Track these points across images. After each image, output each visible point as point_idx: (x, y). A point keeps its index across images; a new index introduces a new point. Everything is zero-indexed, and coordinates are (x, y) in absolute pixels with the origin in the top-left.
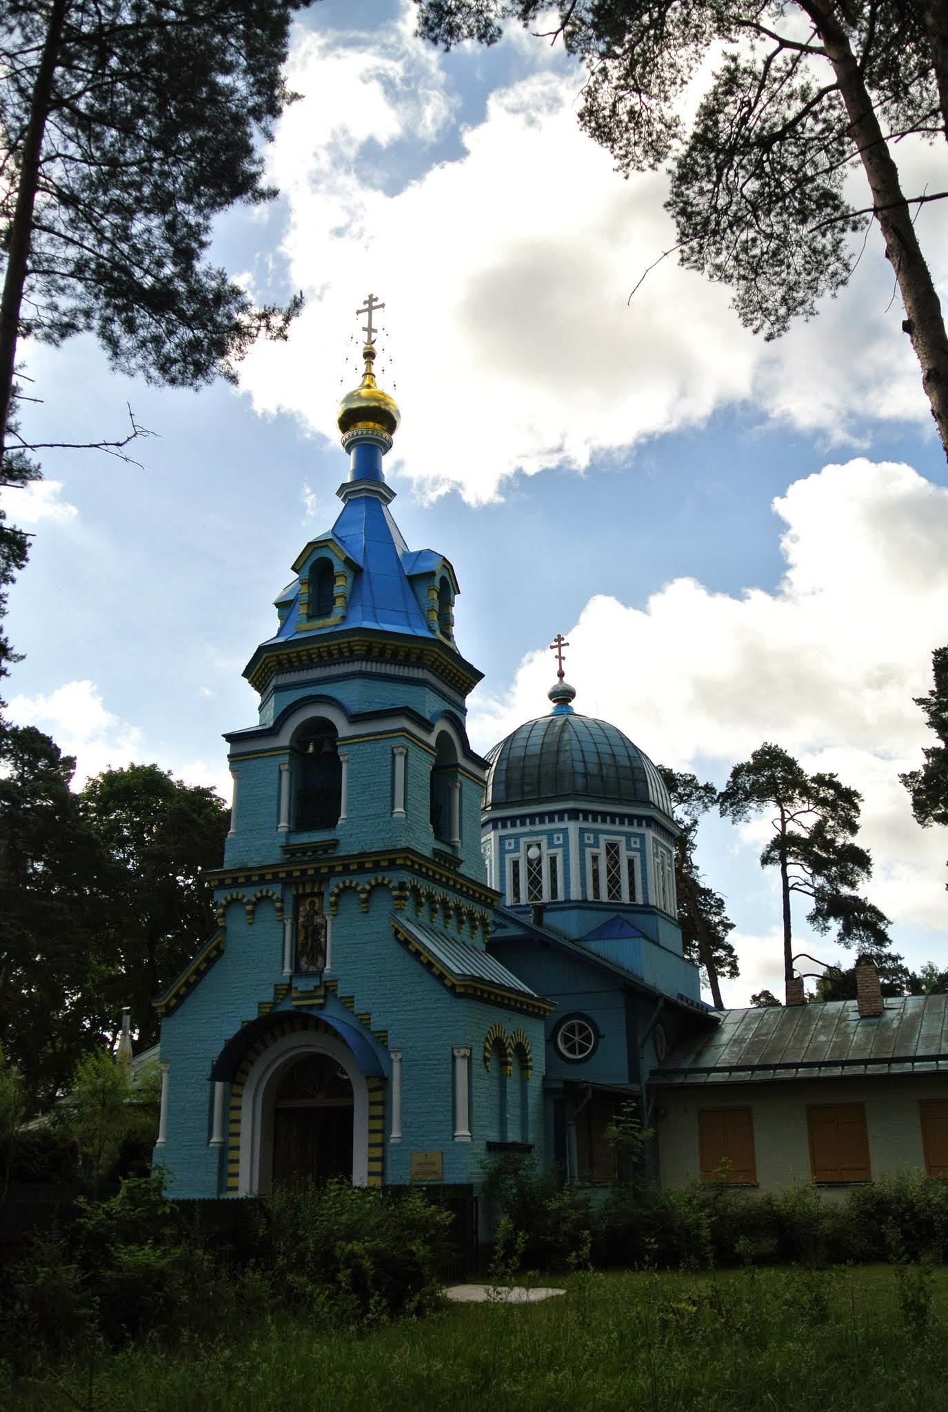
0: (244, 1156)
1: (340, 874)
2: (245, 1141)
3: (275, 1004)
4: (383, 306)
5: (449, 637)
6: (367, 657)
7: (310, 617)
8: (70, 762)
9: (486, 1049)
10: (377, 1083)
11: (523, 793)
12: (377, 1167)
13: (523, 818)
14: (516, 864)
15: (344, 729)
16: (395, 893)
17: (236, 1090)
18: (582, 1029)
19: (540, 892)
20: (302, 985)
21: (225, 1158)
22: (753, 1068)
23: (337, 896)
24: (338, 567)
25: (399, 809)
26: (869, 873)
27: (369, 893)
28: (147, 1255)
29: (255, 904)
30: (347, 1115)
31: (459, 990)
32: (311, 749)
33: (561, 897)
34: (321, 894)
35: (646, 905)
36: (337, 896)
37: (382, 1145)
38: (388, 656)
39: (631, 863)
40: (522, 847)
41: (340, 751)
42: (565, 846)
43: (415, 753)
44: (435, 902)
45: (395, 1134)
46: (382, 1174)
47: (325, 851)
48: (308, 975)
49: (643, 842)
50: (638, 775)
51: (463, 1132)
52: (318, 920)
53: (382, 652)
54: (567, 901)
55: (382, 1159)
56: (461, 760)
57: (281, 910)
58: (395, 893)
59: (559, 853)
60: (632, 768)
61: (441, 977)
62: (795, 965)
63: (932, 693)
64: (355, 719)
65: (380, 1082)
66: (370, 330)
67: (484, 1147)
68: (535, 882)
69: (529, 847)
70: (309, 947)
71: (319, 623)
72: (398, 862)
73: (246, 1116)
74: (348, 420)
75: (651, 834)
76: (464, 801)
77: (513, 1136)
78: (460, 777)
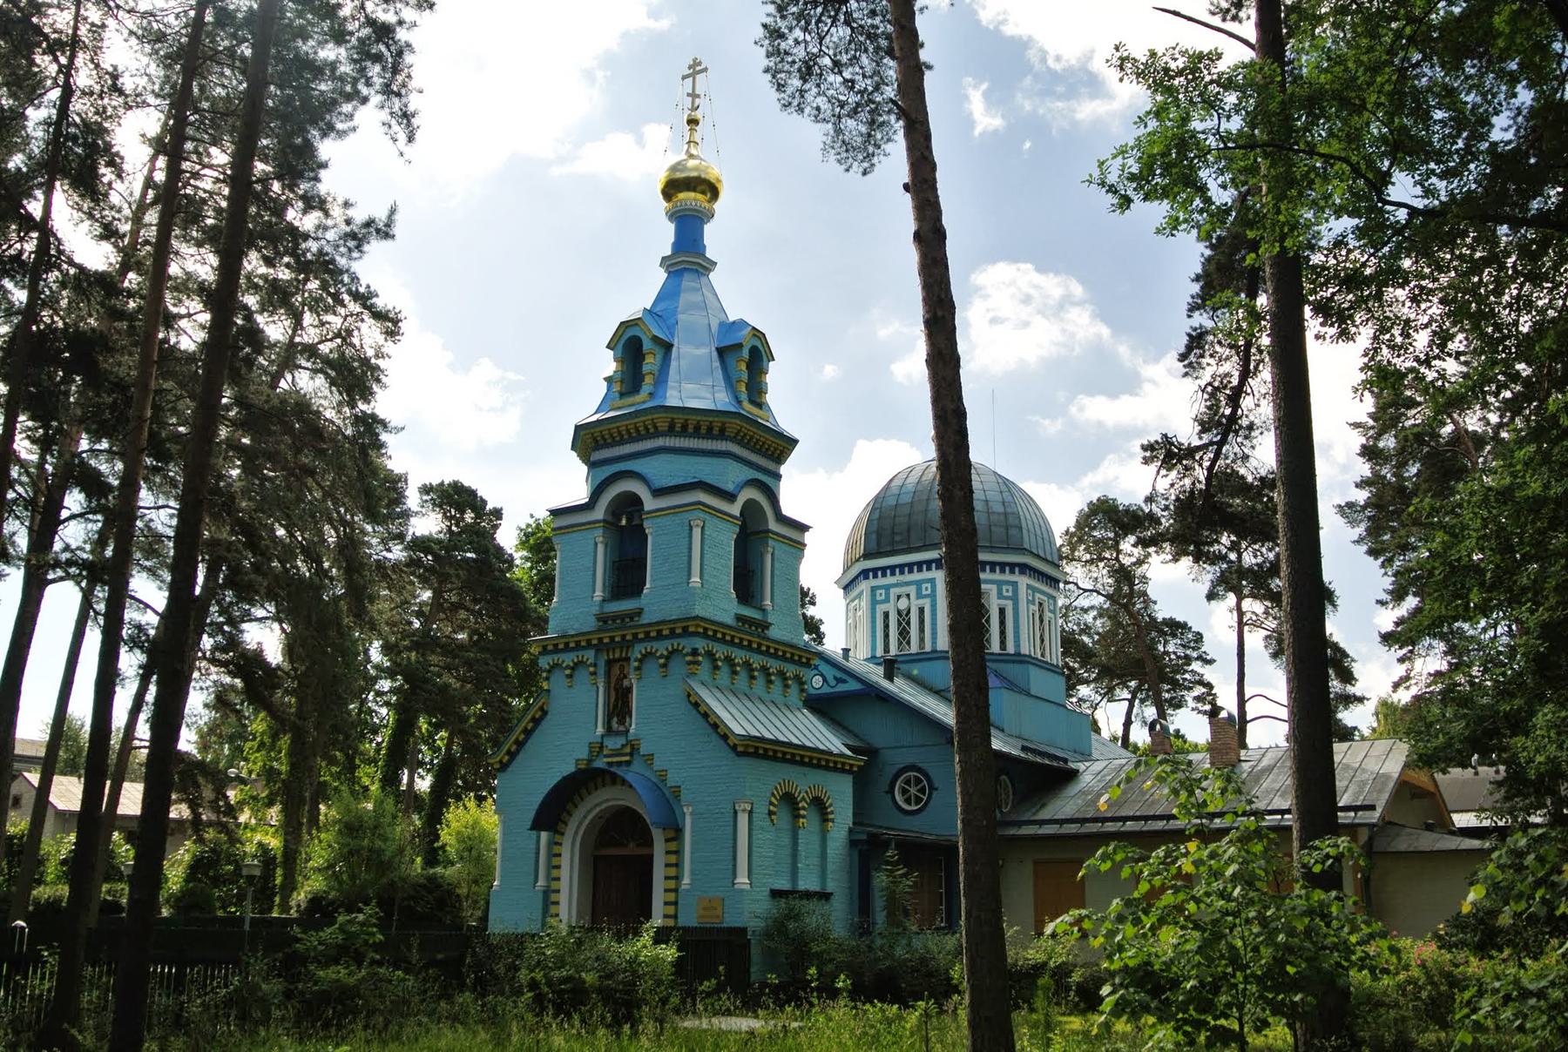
0: (563, 898)
1: (642, 640)
2: (564, 885)
3: (590, 761)
4: (706, 70)
5: (760, 405)
6: (671, 431)
7: (622, 395)
8: (498, 513)
9: (771, 803)
10: (672, 834)
11: (893, 542)
12: (671, 910)
13: (893, 568)
14: (886, 615)
15: (649, 503)
16: (689, 658)
17: (558, 838)
18: (918, 781)
19: (909, 643)
20: (613, 743)
21: (548, 900)
22: (1084, 821)
23: (640, 661)
24: (647, 345)
25: (696, 579)
26: (1335, 606)
27: (667, 658)
28: (338, 973)
29: (573, 669)
30: (648, 861)
31: (740, 749)
32: (624, 522)
33: (928, 648)
34: (627, 659)
35: (1018, 654)
36: (640, 661)
37: (676, 890)
38: (691, 430)
39: (1002, 611)
40: (892, 598)
41: (646, 524)
42: (933, 596)
43: (712, 523)
44: (735, 665)
45: (686, 880)
46: (675, 917)
47: (632, 619)
48: (618, 733)
49: (1016, 591)
50: (1011, 520)
51: (742, 879)
52: (626, 683)
53: (685, 427)
54: (934, 651)
55: (676, 903)
56: (773, 525)
57: (594, 673)
58: (689, 658)
59: (926, 603)
60: (1005, 514)
61: (725, 737)
62: (1248, 706)
63: (1371, 415)
64: (658, 492)
65: (675, 833)
66: (693, 95)
67: (767, 893)
68: (904, 634)
69: (899, 597)
70: (619, 707)
71: (630, 400)
72: (691, 629)
73: (565, 861)
74: (672, 188)
75: (1024, 581)
76: (777, 565)
77: (808, 883)
78: (771, 542)
